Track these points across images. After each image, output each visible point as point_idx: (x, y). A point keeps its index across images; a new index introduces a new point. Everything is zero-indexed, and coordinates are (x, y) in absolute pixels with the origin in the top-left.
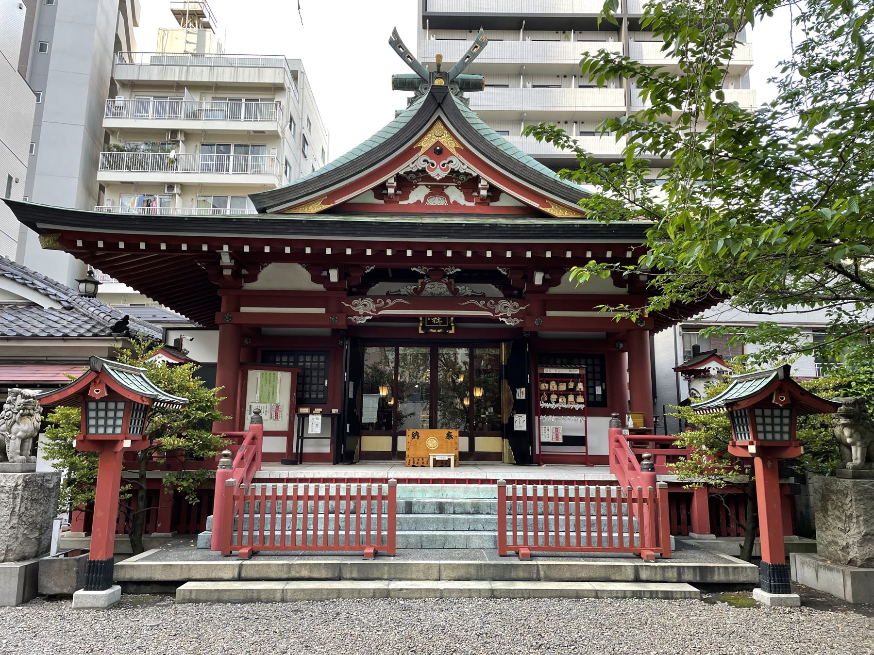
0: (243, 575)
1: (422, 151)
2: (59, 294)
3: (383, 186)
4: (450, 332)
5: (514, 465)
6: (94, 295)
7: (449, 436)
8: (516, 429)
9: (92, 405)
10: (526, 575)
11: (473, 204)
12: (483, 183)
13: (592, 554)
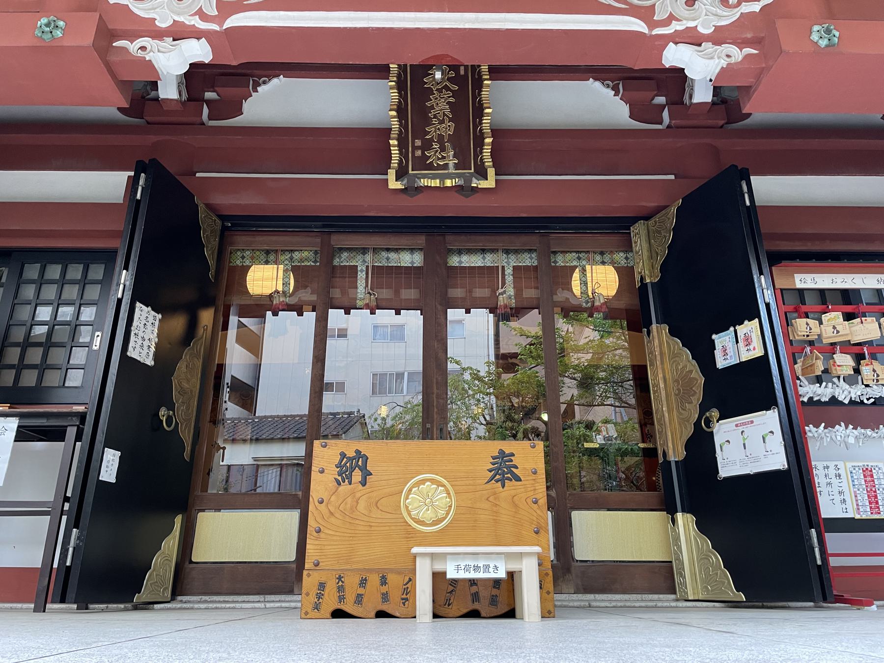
4: (483, 184)
5: (735, 605)
8: (725, 471)
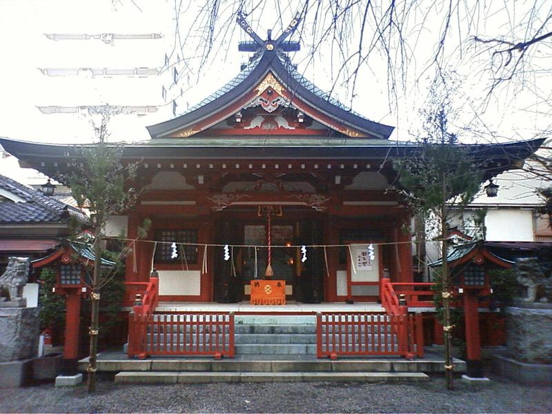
0: (153, 368)
1: (259, 94)
2: (24, 193)
3: (234, 117)
6: (51, 194)
7: (279, 285)
9: (63, 267)
10: (325, 369)
11: (294, 128)
12: (300, 114)
13: (180, 355)
